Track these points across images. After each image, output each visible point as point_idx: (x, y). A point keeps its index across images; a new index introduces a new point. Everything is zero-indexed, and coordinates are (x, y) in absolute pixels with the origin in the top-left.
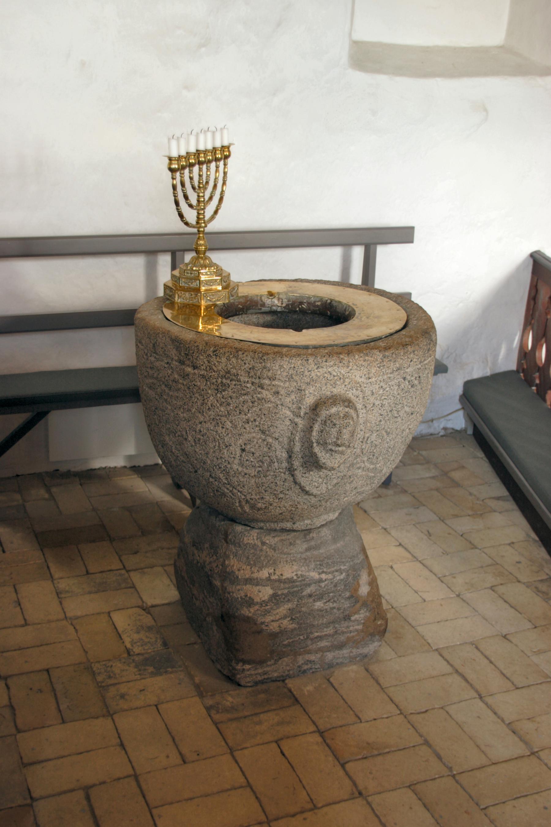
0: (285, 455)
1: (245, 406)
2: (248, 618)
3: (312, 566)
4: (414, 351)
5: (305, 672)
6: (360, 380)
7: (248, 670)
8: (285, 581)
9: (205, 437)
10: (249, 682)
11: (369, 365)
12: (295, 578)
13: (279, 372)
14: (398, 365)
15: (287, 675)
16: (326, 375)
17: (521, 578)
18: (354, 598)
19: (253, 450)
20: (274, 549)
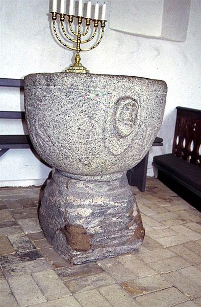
0: (101, 131)
1: (81, 103)
2: (79, 225)
3: (111, 199)
5: (106, 257)
7: (79, 255)
8: (98, 206)
9: (59, 123)
10: (79, 262)
12: (103, 204)
13: (99, 84)
15: (98, 259)
17: (193, 220)
18: (131, 218)
19: (84, 128)
20: (92, 190)
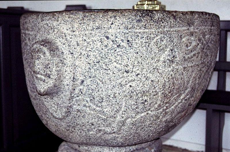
4: (115, 17)
6: (66, 32)
11: (72, 21)
14: (97, 25)
16: (45, 26)
